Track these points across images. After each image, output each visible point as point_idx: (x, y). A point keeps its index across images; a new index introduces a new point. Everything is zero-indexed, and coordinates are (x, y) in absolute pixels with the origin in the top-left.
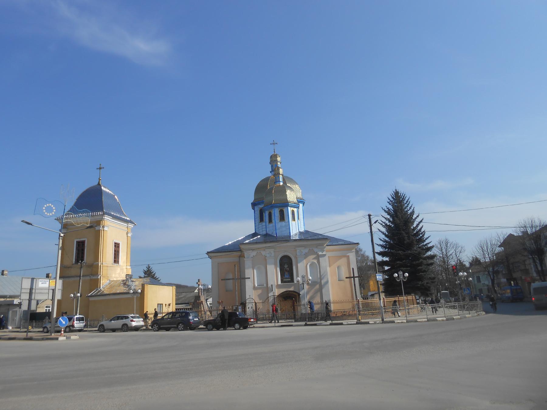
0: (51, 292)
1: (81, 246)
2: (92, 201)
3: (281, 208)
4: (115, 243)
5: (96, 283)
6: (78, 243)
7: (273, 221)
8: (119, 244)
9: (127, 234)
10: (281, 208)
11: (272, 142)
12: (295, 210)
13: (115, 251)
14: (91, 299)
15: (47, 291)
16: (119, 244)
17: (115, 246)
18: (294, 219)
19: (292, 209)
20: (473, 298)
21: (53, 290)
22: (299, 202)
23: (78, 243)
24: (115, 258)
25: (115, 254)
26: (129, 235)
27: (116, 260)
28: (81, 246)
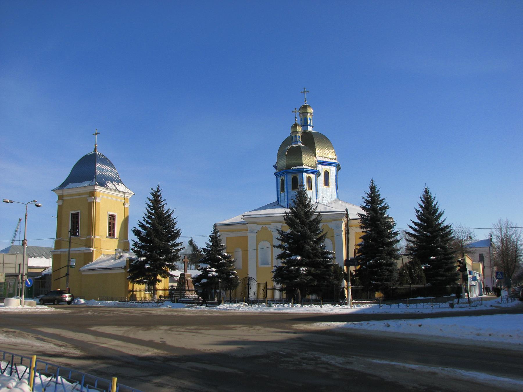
0: (18, 266)
1: (75, 217)
2: (85, 171)
3: (295, 175)
4: (110, 215)
5: (89, 257)
6: (73, 215)
7: (285, 190)
8: (114, 216)
9: (124, 204)
10: (295, 175)
11: (303, 90)
12: (313, 176)
13: (110, 223)
14: (84, 273)
15: (14, 266)
16: (114, 216)
17: (110, 219)
18: (310, 187)
19: (308, 175)
20: (474, 301)
21: (20, 265)
22: (62, 200)
23: (73, 215)
24: (110, 231)
25: (110, 227)
26: (127, 206)
27: (112, 233)
28: (75, 217)
